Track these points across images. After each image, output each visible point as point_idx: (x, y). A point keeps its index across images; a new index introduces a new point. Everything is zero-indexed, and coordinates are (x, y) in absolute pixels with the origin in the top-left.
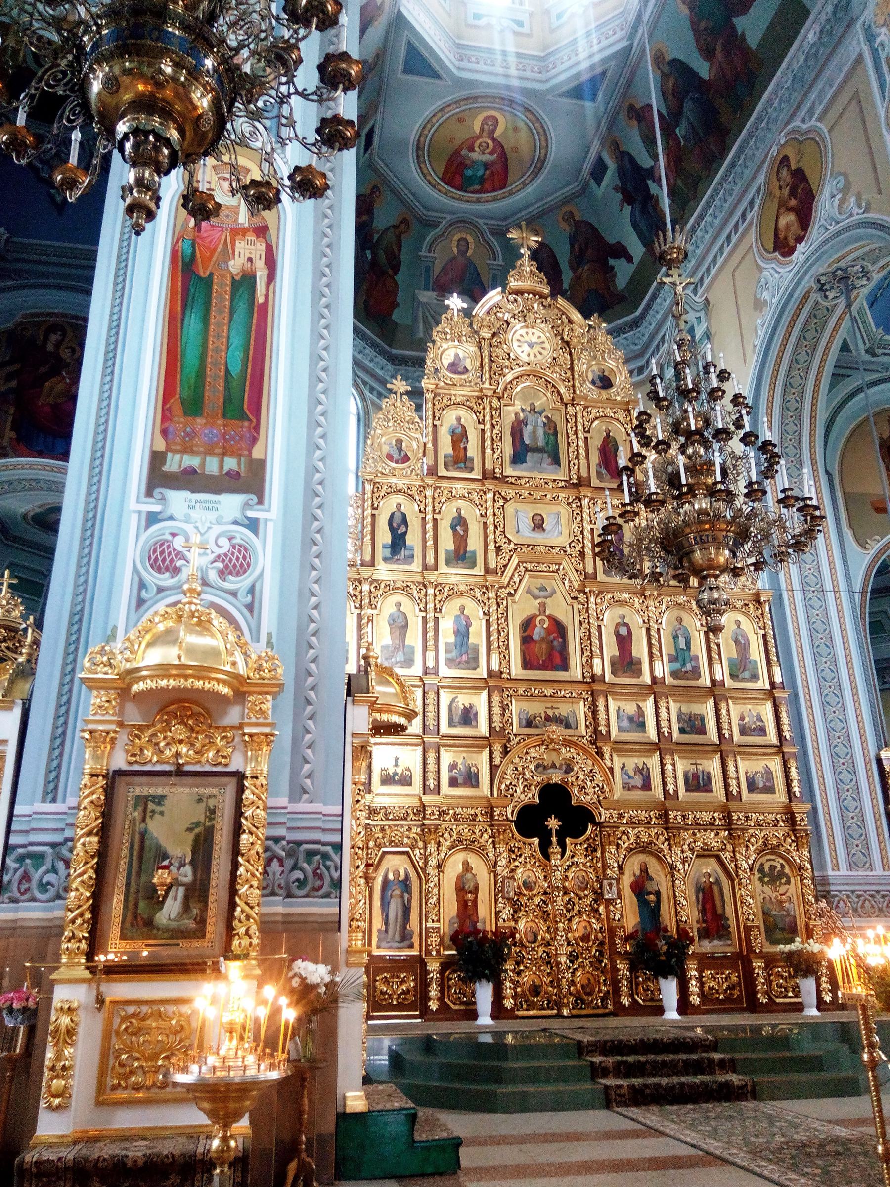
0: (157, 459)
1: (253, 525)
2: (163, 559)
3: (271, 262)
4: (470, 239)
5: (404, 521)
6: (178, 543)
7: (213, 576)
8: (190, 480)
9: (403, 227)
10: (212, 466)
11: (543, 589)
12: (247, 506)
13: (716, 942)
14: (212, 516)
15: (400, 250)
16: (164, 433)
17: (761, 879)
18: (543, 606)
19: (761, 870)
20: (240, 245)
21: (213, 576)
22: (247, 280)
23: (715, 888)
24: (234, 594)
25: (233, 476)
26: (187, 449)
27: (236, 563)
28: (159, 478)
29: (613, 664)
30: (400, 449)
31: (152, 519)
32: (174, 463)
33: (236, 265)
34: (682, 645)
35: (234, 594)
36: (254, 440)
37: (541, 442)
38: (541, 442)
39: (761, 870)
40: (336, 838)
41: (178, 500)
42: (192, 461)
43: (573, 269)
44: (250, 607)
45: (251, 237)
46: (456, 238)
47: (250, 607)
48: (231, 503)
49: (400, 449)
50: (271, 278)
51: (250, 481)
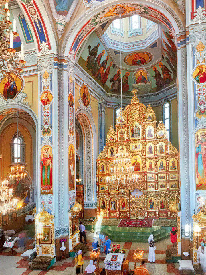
0: (41, 191)
1: (52, 198)
2: (43, 202)
3: (52, 162)
4: (142, 72)
5: (113, 150)
6: (44, 201)
7: (48, 204)
8: (45, 193)
9: (127, 75)
10: (47, 191)
11: (136, 158)
12: (51, 196)
13: (163, 209)
14: (47, 197)
15: (127, 79)
16: (42, 187)
17: (172, 201)
18: (136, 161)
19: (172, 199)
20: (48, 160)
21: (48, 204)
22: (49, 165)
23: (164, 202)
24: (50, 206)
25: (49, 192)
26: (44, 189)
27: (50, 203)
28: (42, 194)
29: (148, 169)
30: (112, 138)
31: (41, 198)
32: (43, 191)
33: (48, 164)
34: (162, 165)
35: (50, 206)
36: (51, 187)
37: (137, 132)
38: (137, 132)
39: (172, 199)
40: (68, 227)
41: (44, 195)
42: (45, 191)
43: (163, 75)
44: (52, 208)
45: (49, 159)
46: (139, 72)
47: (52, 208)
48: (49, 195)
49: (112, 138)
50: (52, 165)
51: (51, 193)
